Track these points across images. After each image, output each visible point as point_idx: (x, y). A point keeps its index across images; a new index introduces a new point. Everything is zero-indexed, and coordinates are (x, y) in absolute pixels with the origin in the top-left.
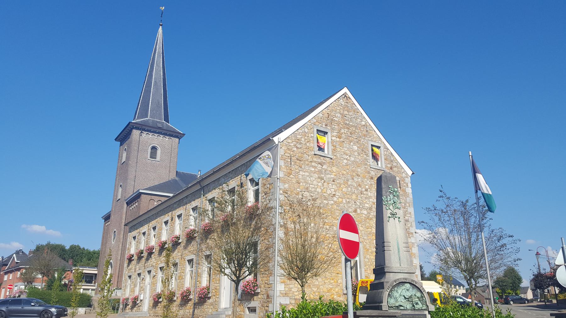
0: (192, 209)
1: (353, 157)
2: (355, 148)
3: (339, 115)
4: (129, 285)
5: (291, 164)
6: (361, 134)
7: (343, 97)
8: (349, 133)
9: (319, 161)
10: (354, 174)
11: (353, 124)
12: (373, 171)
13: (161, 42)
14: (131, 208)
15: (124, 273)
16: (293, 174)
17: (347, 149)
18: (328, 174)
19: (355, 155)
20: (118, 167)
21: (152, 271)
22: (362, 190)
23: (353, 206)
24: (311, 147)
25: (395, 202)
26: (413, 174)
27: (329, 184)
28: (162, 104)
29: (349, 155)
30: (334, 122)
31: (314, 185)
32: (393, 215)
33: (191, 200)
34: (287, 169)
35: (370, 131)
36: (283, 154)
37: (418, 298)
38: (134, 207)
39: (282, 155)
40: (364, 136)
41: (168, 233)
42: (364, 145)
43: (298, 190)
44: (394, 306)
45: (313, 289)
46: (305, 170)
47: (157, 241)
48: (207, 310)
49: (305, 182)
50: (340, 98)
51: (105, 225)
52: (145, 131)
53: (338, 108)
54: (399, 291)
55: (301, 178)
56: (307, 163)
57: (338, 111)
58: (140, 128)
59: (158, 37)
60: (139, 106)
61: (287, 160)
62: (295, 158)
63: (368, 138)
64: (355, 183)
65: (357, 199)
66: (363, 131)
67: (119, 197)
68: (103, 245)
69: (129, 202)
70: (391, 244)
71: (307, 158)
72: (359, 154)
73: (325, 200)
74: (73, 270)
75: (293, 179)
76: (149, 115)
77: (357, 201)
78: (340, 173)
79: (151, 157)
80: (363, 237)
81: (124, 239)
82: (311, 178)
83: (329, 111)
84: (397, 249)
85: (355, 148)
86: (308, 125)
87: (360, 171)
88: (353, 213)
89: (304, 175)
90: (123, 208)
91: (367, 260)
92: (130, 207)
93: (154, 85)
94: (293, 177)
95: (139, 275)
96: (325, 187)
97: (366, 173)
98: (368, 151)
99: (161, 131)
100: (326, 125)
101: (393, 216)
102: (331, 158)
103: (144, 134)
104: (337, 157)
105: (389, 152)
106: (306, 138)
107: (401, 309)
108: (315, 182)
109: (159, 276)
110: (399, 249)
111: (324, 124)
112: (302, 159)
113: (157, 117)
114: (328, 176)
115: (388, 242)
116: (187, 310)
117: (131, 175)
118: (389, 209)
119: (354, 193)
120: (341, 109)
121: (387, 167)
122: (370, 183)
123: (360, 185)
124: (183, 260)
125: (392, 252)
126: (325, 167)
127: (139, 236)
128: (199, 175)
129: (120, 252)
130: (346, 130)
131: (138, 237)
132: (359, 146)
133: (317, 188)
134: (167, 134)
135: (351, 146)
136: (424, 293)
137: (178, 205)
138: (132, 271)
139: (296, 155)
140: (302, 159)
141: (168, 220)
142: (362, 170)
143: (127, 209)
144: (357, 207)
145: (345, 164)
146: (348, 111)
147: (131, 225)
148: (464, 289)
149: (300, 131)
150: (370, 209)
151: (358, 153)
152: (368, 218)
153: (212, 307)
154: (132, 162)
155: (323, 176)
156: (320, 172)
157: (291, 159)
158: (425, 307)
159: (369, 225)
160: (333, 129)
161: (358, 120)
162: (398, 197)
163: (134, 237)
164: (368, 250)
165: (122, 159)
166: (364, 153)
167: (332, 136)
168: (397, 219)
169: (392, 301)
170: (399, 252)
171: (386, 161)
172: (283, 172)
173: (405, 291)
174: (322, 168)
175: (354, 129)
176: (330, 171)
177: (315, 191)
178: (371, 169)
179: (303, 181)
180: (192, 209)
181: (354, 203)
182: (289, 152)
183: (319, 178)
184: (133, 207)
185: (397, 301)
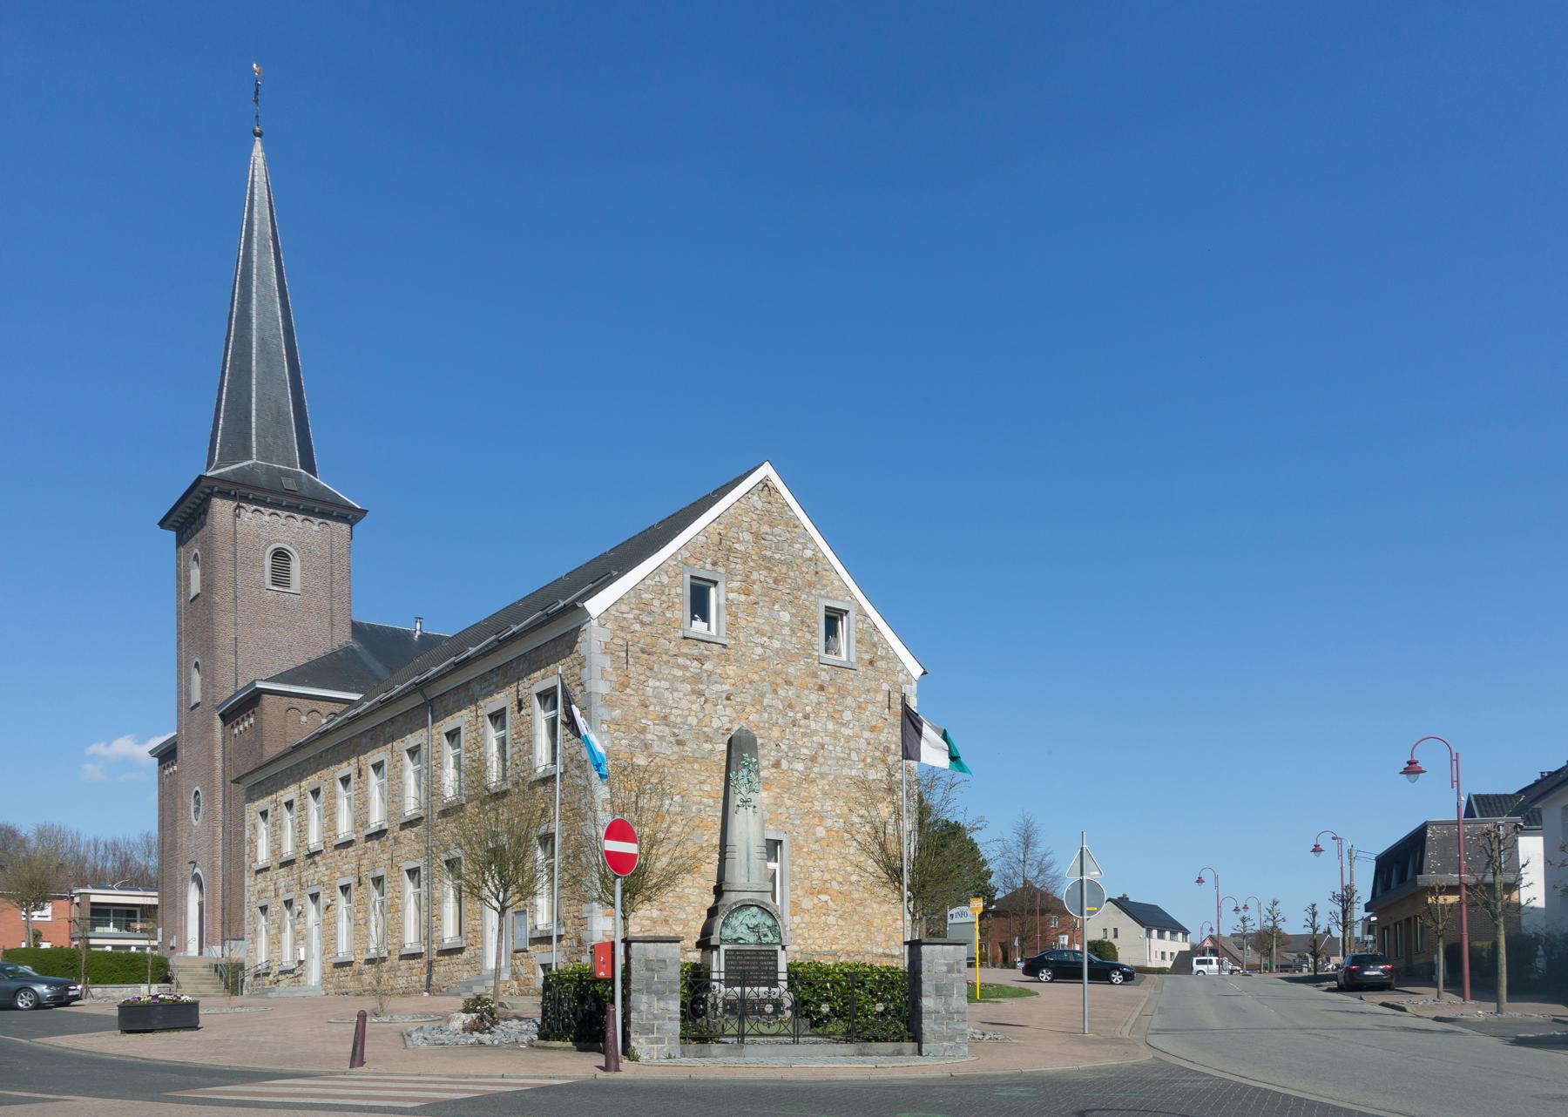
0: (409, 751)
1: (778, 640)
3: (747, 536)
4: (264, 929)
5: (627, 662)
6: (800, 582)
7: (761, 488)
8: (770, 581)
9: (695, 652)
10: (779, 680)
12: (825, 670)
13: (264, 198)
14: (236, 731)
16: (633, 686)
18: (716, 683)
19: (783, 635)
20: (179, 608)
21: (321, 894)
22: (795, 717)
23: (773, 753)
24: (677, 620)
26: (925, 673)
28: (289, 413)
29: (769, 635)
30: (735, 555)
31: (682, 710)
33: (404, 729)
35: (824, 573)
36: (608, 640)
37: (768, 927)
38: (245, 729)
39: (606, 644)
40: (810, 586)
41: (352, 805)
42: (808, 608)
43: (644, 721)
45: (674, 927)
46: (660, 676)
47: (325, 825)
48: (458, 973)
49: (660, 703)
50: (751, 492)
51: (161, 772)
52: (250, 501)
53: (745, 519)
55: (651, 694)
56: (665, 658)
57: (745, 525)
58: (233, 493)
59: (253, 176)
60: (221, 422)
61: (617, 653)
62: (638, 649)
63: (819, 591)
64: (779, 702)
65: (784, 738)
66: (807, 573)
67: (196, 697)
68: (165, 829)
69: (228, 711)
70: (736, 849)
71: (667, 647)
72: (793, 632)
74: (77, 895)
75: (632, 698)
76: (254, 451)
77: (781, 742)
79: (275, 583)
80: (790, 821)
82: (675, 694)
83: (722, 527)
87: (793, 672)
88: (771, 770)
89: (659, 687)
90: (211, 729)
91: (796, 869)
92: (233, 727)
93: (261, 351)
94: (633, 692)
95: (289, 904)
96: (707, 712)
97: (808, 676)
98: (816, 623)
99: (297, 502)
100: (714, 564)
102: (725, 646)
103: (248, 513)
105: (868, 623)
106: (664, 598)
108: (684, 703)
109: (341, 907)
111: (709, 560)
112: (654, 649)
113: (278, 456)
114: (717, 688)
116: (414, 978)
117: (225, 637)
118: (740, 792)
119: (777, 723)
121: (862, 659)
123: (791, 706)
124: (395, 869)
125: (736, 861)
126: (708, 666)
127: (276, 810)
128: (418, 633)
130: (764, 573)
131: (275, 813)
132: (794, 611)
134: (313, 511)
137: (372, 739)
138: (268, 894)
139: (638, 642)
140: (654, 649)
141: (350, 775)
143: (223, 732)
144: (782, 757)
145: (758, 658)
146: (770, 526)
147: (249, 782)
148: (1186, 941)
150: (812, 760)
151: (792, 629)
152: (805, 779)
153: (468, 967)
154: (222, 597)
155: (702, 687)
156: (696, 678)
157: (627, 650)
158: (777, 940)
159: (806, 794)
160: (730, 574)
163: (261, 813)
164: (801, 848)
165: (188, 586)
169: (728, 933)
170: (748, 860)
171: (859, 645)
172: (608, 683)
173: (751, 917)
174: (701, 668)
175: (784, 570)
176: (720, 675)
178: (822, 666)
179: (655, 701)
180: (409, 751)
181: (774, 747)
182: (623, 635)
183: (693, 692)
184: (241, 728)
185: (735, 932)
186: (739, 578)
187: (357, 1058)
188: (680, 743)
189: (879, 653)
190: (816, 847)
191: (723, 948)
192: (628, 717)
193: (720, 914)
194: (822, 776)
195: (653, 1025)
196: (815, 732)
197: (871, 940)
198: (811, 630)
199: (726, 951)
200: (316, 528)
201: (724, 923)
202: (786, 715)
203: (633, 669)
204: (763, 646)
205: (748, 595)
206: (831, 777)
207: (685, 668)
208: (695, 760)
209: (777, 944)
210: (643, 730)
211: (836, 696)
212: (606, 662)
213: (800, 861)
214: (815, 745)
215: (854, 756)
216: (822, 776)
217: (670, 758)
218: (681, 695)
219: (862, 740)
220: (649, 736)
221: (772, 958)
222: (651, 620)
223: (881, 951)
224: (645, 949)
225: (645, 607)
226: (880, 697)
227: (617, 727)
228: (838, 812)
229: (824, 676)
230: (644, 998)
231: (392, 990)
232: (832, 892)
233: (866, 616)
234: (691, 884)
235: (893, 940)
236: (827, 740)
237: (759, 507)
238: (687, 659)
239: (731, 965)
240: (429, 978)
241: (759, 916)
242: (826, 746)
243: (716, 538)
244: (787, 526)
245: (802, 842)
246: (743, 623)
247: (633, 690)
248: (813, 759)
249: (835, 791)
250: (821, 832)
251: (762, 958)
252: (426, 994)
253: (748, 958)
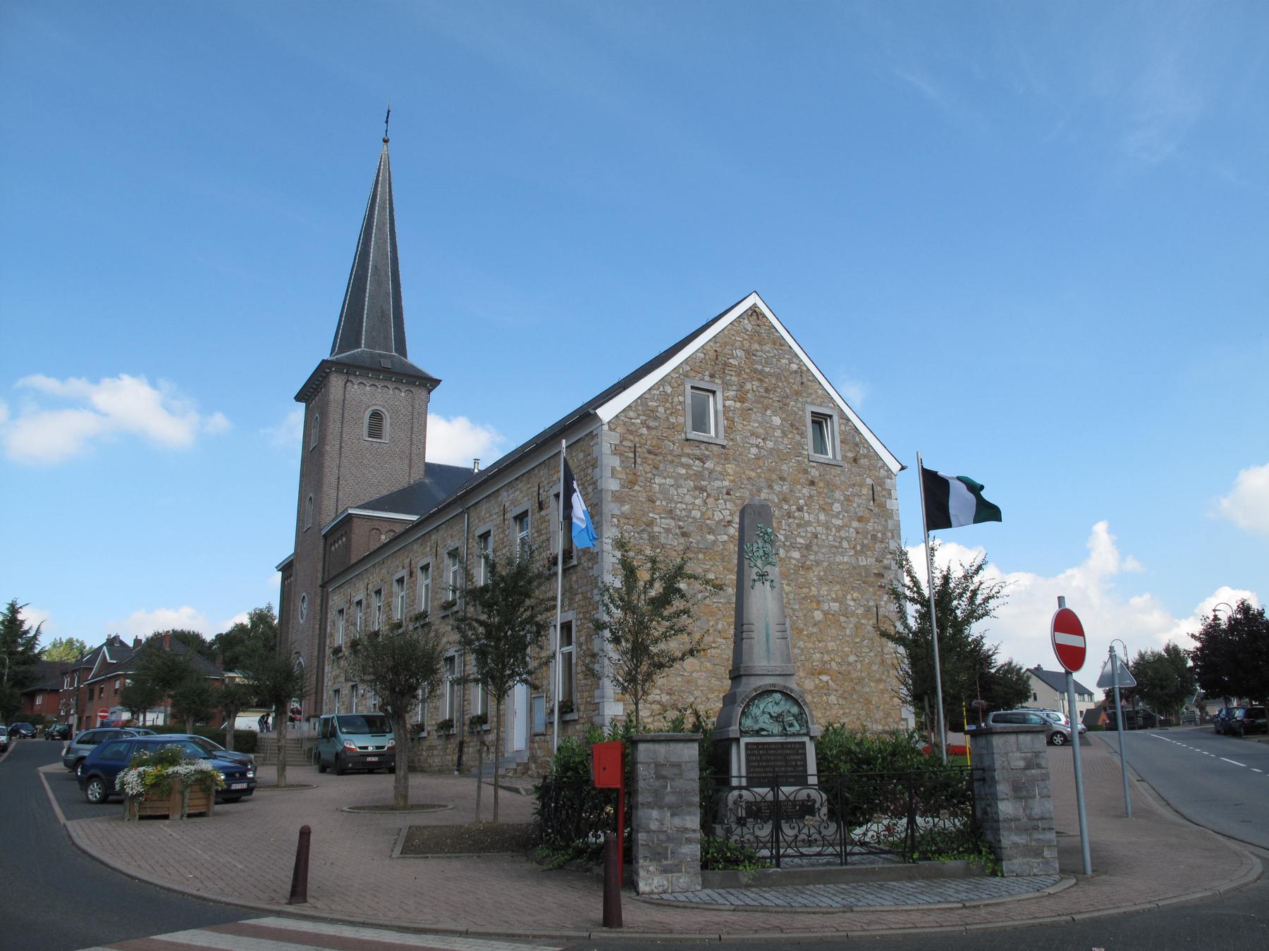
1: (771, 441)
2: (777, 421)
3: (740, 353)
8: (762, 390)
9: (697, 452)
11: (772, 371)
12: (814, 467)
15: (325, 684)
16: (640, 484)
17: (757, 425)
18: (717, 479)
27: (717, 500)
29: (763, 437)
32: (762, 576)
34: (627, 474)
35: (809, 383)
36: (618, 442)
37: (794, 715)
39: (616, 445)
42: (796, 414)
43: (651, 515)
46: (665, 475)
49: (665, 499)
56: (670, 458)
62: (645, 450)
64: (775, 497)
66: (794, 384)
72: (784, 434)
73: (709, 533)
75: (639, 494)
78: (743, 476)
81: (324, 613)
84: (764, 635)
85: (777, 421)
86: (672, 378)
89: (664, 484)
94: (641, 489)
97: (799, 473)
100: (712, 376)
102: (723, 447)
108: (688, 499)
110: (767, 635)
111: (707, 373)
112: (660, 450)
114: (717, 484)
118: (756, 565)
120: (744, 339)
122: (807, 494)
123: (785, 500)
126: (709, 465)
129: (317, 641)
132: (784, 416)
133: (693, 509)
135: (767, 418)
139: (646, 444)
140: (660, 450)
142: (792, 467)
149: (655, 392)
150: (807, 549)
156: (699, 476)
158: (804, 731)
159: (803, 580)
164: (801, 631)
166: (795, 432)
167: (726, 399)
168: (768, 584)
169: (748, 723)
171: (844, 445)
173: (773, 705)
174: (703, 467)
177: (688, 517)
179: (661, 496)
182: (632, 438)
183: (696, 488)
186: (734, 388)
187: (299, 890)
188: (684, 535)
189: (861, 452)
190: (815, 630)
191: (744, 741)
192: (637, 512)
193: (738, 702)
194: (818, 563)
195: (667, 848)
196: (808, 523)
197: (871, 718)
198: (800, 432)
199: (747, 744)
200: (403, 394)
201: (743, 713)
202: (782, 508)
203: (641, 468)
204: (757, 446)
205: (743, 402)
206: (826, 564)
207: (688, 467)
208: (700, 550)
209: (804, 735)
210: (651, 523)
211: (826, 490)
212: (615, 462)
213: (801, 644)
214: (809, 535)
215: (845, 544)
216: (818, 563)
217: (676, 548)
218: (685, 491)
219: (851, 530)
220: (656, 529)
221: (800, 751)
222: (657, 424)
223: (880, 727)
224: (655, 752)
225: (651, 413)
226: (865, 491)
227: (626, 521)
228: (834, 596)
229: (814, 473)
230: (655, 813)
231: (430, 766)
232: (831, 672)
233: (848, 420)
234: (698, 668)
235: (892, 717)
236: (819, 529)
237: (750, 329)
238: (690, 458)
240: (460, 757)
241: (782, 702)
242: (819, 536)
243: (712, 354)
244: (775, 344)
245: (802, 626)
246: (740, 427)
247: (640, 486)
248: (808, 547)
249: (830, 577)
250: (818, 615)
251: (788, 752)
252: (456, 773)
253: (772, 752)
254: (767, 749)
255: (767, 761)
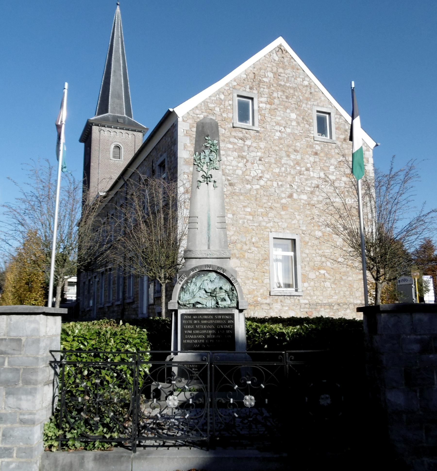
2: (293, 116)
9: (241, 135)
12: (318, 144)
23: (289, 190)
25: (211, 159)
26: (377, 145)
29: (284, 125)
30: (263, 84)
44: (187, 303)
54: (198, 284)
72: (298, 123)
79: (114, 157)
85: (293, 116)
100: (251, 88)
101: (206, 179)
102: (258, 132)
104: (266, 128)
106: (222, 106)
107: (198, 307)
108: (234, 163)
110: (209, 225)
111: (248, 87)
114: (253, 154)
115: (194, 217)
123: (298, 164)
126: (248, 142)
136: (235, 284)
142: (303, 144)
155: (244, 154)
156: (241, 149)
160: (260, 94)
161: (298, 79)
162: (217, 151)
169: (186, 297)
171: (338, 131)
183: (239, 156)
239: (188, 329)
251: (218, 322)
254: (200, 320)
255: (201, 329)
